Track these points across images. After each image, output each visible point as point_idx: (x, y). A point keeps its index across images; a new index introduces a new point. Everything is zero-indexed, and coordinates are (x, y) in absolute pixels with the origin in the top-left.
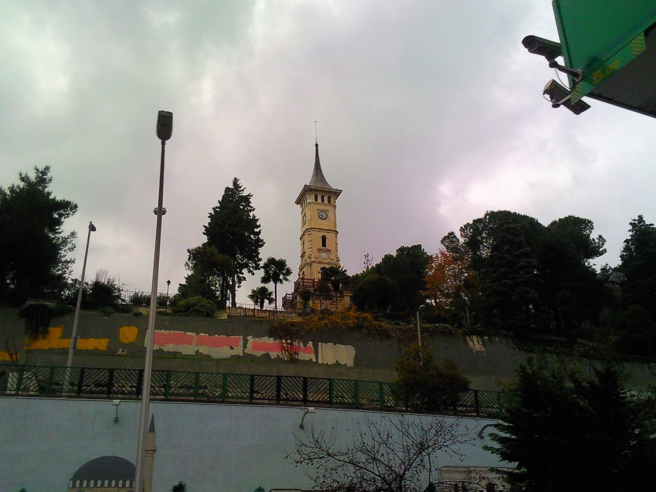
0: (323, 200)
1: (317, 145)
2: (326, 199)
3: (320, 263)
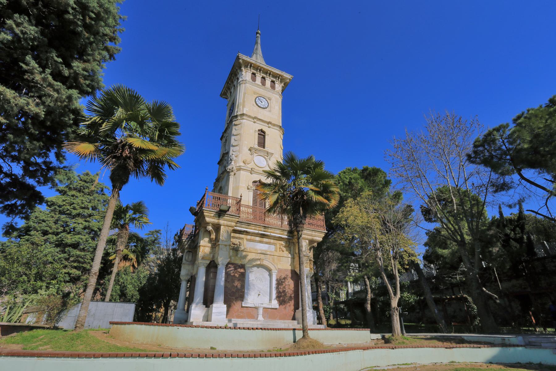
0: (263, 83)
3: (252, 171)
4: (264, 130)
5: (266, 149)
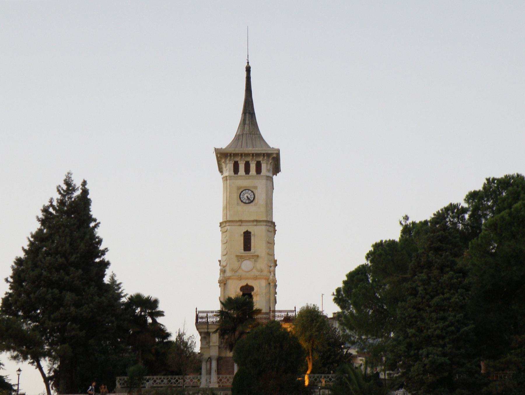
0: (247, 170)
1: (248, 69)
2: (253, 167)
4: (249, 230)
5: (274, 177)
